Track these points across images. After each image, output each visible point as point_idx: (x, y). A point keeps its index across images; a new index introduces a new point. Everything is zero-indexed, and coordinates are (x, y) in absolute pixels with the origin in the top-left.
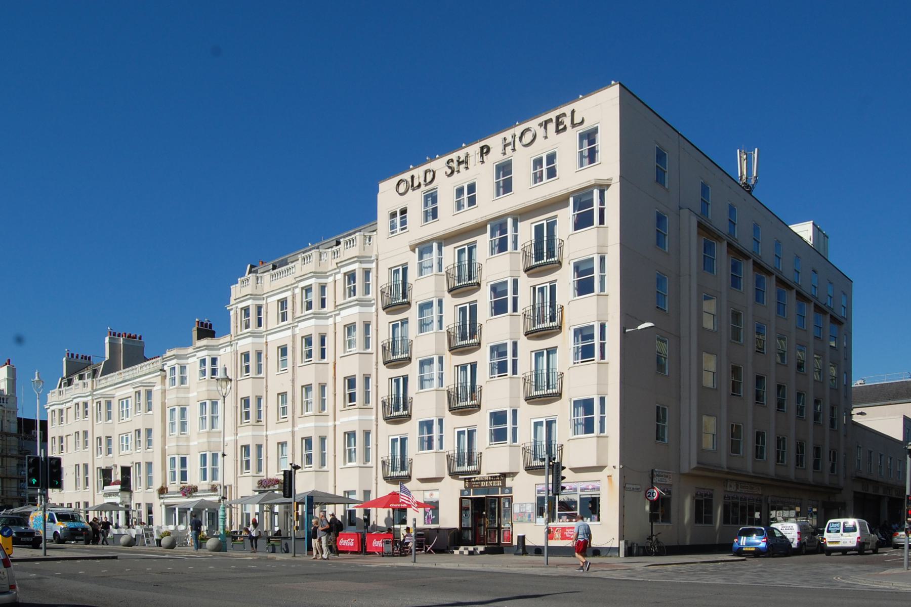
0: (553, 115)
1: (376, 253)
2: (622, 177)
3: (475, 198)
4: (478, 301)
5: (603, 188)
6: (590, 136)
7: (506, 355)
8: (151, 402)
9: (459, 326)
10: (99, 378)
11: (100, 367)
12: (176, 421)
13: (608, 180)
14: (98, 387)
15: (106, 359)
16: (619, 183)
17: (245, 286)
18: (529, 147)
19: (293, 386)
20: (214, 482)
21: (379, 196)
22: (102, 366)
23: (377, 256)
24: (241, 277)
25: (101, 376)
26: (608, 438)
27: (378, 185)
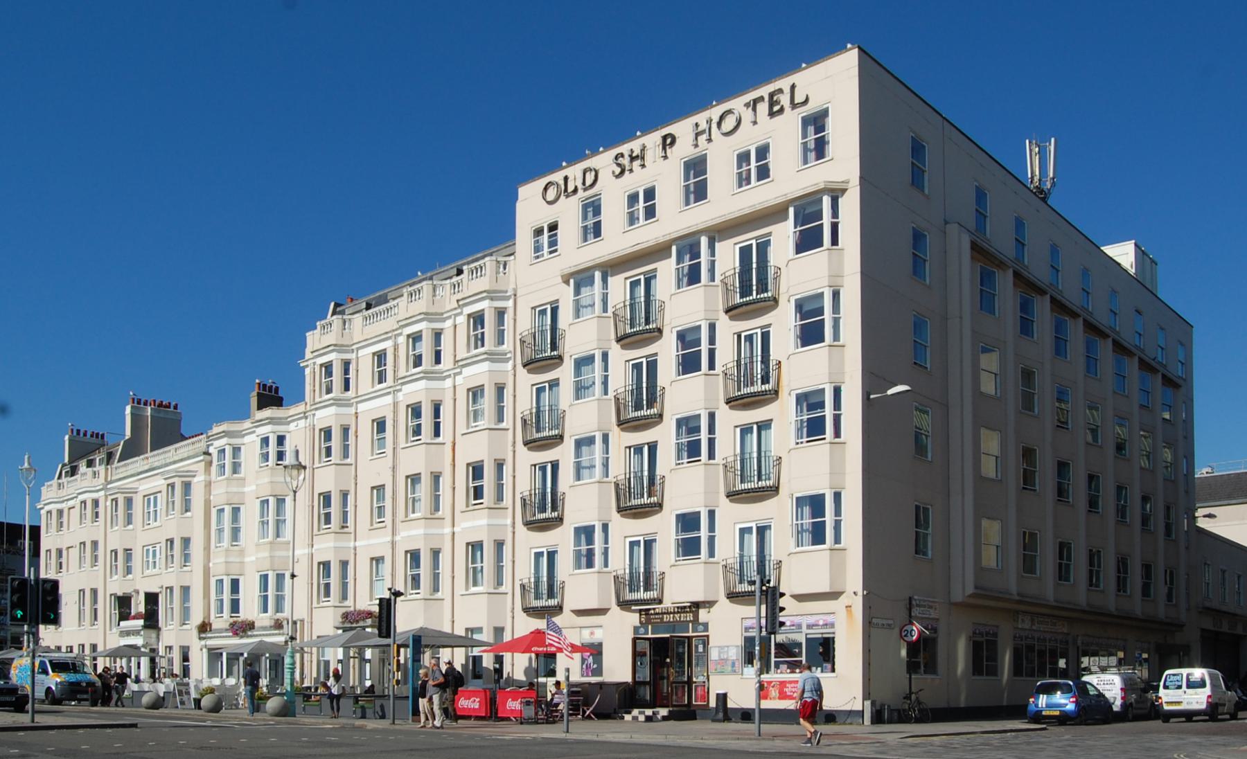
0: (764, 91)
5: (836, 194)
6: (817, 121)
7: (699, 431)
9: (632, 390)
13: (843, 182)
14: (114, 478)
21: (519, 206)
24: (320, 320)
25: (119, 462)
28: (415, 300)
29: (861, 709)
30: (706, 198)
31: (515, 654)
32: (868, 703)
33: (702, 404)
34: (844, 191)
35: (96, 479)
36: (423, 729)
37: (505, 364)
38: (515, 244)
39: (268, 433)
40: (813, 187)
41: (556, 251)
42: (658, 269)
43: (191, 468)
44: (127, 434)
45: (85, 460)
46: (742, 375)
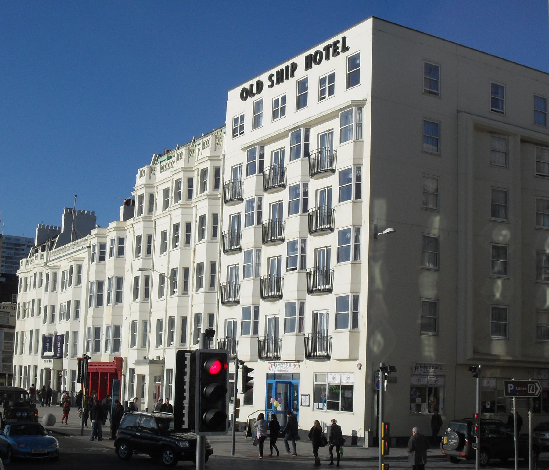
0: (331, 41)
1: (224, 154)
2: (373, 97)
3: (244, 116)
4: (332, 186)
5: (360, 106)
6: (354, 62)
7: (297, 250)
8: (81, 275)
9: (269, 223)
10: (54, 250)
11: (56, 240)
12: (94, 294)
13: (363, 100)
14: (52, 258)
15: (62, 232)
16: (371, 103)
17: (164, 171)
18: (297, 70)
19: (194, 258)
20: (117, 354)
21: (228, 103)
22: (57, 239)
23: (224, 156)
24: (140, 168)
25: (55, 249)
26: (360, 333)
27: (228, 93)
28: (206, 147)
29: (364, 437)
30: (359, 83)
31: (320, 403)
32: (367, 433)
33: (350, 223)
34: (364, 105)
35: (42, 259)
36: (261, 460)
37: (105, 238)
38: (225, 128)
39: (171, 223)
40: (330, 110)
41: (243, 133)
42: (285, 147)
43: (56, 264)
44: (62, 231)
45: (41, 246)
46: (319, 215)
